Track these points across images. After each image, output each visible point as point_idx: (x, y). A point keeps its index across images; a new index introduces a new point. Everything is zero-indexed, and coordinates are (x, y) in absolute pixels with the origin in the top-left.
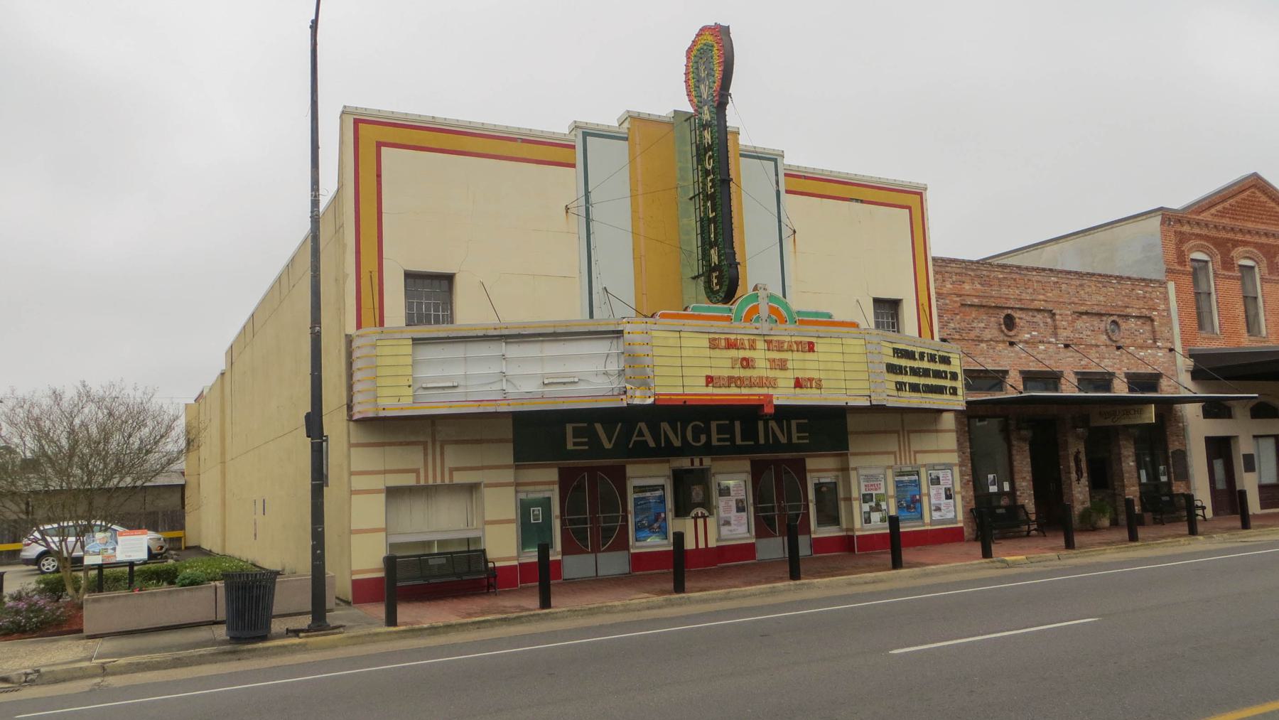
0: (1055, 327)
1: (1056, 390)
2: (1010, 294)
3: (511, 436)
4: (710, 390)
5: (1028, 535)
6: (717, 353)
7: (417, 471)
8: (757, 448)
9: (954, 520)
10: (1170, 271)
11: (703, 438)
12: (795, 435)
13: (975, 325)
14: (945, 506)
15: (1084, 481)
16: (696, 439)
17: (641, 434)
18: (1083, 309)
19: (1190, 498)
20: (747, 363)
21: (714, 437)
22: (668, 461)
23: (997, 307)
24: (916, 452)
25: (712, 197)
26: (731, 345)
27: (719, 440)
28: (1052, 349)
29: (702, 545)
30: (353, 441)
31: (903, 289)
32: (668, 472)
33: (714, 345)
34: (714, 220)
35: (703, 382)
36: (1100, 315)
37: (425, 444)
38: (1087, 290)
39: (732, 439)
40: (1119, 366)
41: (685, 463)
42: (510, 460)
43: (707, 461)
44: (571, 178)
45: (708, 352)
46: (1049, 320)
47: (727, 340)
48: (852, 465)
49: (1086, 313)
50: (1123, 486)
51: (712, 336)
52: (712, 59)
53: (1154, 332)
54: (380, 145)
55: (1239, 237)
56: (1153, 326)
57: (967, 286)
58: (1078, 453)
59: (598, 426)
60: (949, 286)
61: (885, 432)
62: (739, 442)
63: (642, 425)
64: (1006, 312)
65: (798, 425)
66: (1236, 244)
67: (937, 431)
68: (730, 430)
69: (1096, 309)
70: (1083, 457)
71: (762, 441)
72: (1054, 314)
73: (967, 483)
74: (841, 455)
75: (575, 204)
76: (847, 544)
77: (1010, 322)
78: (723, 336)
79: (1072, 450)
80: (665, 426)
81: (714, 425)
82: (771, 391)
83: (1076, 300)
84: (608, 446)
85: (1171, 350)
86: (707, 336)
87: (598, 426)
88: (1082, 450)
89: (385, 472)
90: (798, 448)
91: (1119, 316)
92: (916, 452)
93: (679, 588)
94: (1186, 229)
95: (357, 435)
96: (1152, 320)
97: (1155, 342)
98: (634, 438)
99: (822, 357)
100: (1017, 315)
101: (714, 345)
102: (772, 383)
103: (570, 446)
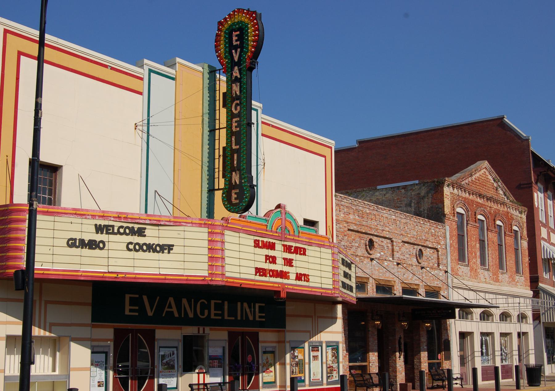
0: (393, 251)
3: (90, 301)
4: (258, 278)
6: (258, 250)
8: (235, 323)
11: (206, 312)
12: (258, 315)
13: (353, 244)
15: (402, 357)
16: (202, 313)
17: (170, 306)
18: (406, 239)
19: (450, 371)
21: (213, 312)
22: (181, 329)
25: (237, 135)
27: (131, 311)
28: (391, 264)
31: (318, 215)
32: (180, 337)
33: (257, 244)
34: (238, 151)
35: (253, 271)
38: (409, 226)
39: (222, 315)
41: (191, 330)
42: (89, 320)
43: (207, 329)
44: (138, 101)
47: (263, 241)
48: (288, 339)
49: (408, 243)
50: (420, 362)
54: (20, 54)
56: (438, 254)
57: (351, 217)
58: (400, 338)
59: (145, 298)
60: (342, 215)
61: (306, 316)
62: (226, 317)
63: (171, 300)
64: (371, 237)
65: (260, 306)
68: (219, 307)
69: (412, 241)
71: (239, 318)
73: (345, 357)
74: (278, 331)
75: (141, 123)
77: (371, 243)
79: (397, 337)
80: (184, 301)
81: (213, 302)
83: (403, 233)
84: (150, 314)
85: (446, 272)
87: (145, 298)
88: (402, 336)
90: (254, 323)
91: (423, 246)
96: (438, 251)
97: (438, 266)
99: (311, 260)
100: (375, 239)
101: (257, 244)
103: (127, 312)
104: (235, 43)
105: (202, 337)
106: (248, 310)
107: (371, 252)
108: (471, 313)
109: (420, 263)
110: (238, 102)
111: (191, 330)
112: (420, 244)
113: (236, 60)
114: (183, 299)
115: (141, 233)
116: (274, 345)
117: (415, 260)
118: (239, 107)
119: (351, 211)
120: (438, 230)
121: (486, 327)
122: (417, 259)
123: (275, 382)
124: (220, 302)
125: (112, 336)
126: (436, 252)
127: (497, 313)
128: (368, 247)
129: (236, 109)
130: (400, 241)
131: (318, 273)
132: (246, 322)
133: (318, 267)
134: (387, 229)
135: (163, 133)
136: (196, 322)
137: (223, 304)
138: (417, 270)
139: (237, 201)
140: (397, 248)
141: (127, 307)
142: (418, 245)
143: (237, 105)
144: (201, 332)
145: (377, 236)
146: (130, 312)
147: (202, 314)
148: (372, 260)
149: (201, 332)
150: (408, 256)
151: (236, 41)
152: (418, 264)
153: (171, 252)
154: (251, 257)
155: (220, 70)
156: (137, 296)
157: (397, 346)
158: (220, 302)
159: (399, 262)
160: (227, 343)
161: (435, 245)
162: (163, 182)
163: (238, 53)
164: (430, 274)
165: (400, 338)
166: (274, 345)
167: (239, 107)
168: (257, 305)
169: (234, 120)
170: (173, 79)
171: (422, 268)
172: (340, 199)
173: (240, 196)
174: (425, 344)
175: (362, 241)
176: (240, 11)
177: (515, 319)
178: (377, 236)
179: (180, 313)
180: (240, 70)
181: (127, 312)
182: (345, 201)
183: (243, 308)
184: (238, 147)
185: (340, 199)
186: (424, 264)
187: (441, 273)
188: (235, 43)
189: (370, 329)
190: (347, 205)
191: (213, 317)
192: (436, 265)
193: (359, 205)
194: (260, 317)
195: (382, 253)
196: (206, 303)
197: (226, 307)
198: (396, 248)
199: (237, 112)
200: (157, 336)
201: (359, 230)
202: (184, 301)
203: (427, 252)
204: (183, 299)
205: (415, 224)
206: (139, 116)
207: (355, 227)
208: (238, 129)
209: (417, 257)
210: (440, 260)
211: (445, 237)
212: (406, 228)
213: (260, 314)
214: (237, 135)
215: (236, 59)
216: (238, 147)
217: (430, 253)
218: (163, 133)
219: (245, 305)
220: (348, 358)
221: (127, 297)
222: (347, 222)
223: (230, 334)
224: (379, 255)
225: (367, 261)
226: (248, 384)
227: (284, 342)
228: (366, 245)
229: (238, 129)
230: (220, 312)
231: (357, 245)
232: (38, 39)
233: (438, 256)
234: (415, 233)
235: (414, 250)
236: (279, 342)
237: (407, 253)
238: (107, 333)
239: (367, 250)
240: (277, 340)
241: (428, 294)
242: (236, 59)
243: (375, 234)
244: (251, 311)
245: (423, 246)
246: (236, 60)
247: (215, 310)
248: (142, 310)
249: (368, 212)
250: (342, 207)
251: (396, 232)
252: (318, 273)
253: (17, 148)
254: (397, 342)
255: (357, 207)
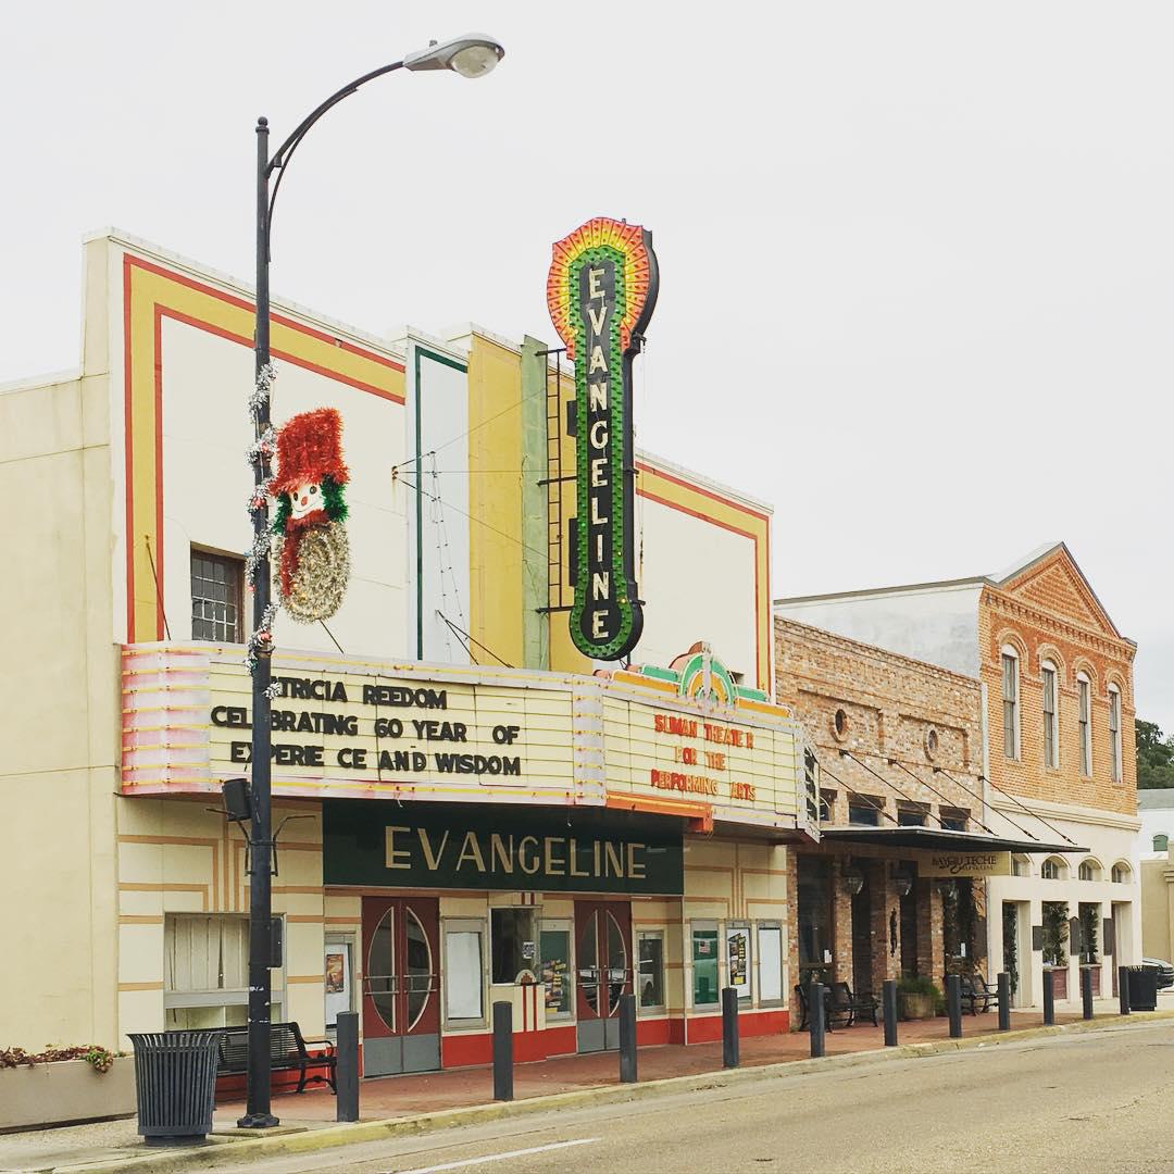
1: (876, 825)
2: (841, 680)
4: (655, 791)
5: (848, 1026)
6: (663, 737)
7: (202, 888)
8: (579, 884)
9: (780, 1003)
10: (985, 668)
11: (537, 860)
12: (631, 866)
14: (771, 976)
15: (898, 951)
17: (469, 851)
18: (906, 711)
20: (688, 756)
21: (549, 861)
22: (487, 896)
23: (831, 698)
24: (749, 901)
25: (604, 495)
26: (677, 728)
27: (397, 860)
29: (530, 1028)
30: (123, 831)
34: (606, 530)
36: (920, 721)
37: (213, 843)
39: (566, 867)
40: (931, 793)
41: (509, 900)
43: (539, 896)
45: (652, 735)
46: (875, 723)
47: (672, 719)
48: (687, 914)
50: (931, 962)
51: (659, 712)
52: (610, 287)
53: (966, 751)
54: (160, 311)
55: (1044, 629)
56: (965, 741)
57: (804, 664)
58: (894, 913)
59: (422, 832)
60: (787, 661)
62: (573, 872)
63: (471, 835)
64: (841, 706)
66: (1042, 638)
67: (769, 872)
68: (565, 854)
70: (898, 920)
71: (597, 874)
72: (881, 715)
74: (667, 900)
76: (673, 1031)
78: (669, 714)
79: (889, 912)
80: (496, 838)
81: (548, 840)
82: (710, 799)
83: (901, 697)
84: (433, 866)
86: (652, 711)
87: (422, 832)
89: (164, 887)
91: (937, 724)
92: (749, 901)
93: (504, 1093)
94: (1000, 611)
95: (130, 822)
97: (966, 765)
98: (463, 857)
100: (848, 710)
102: (702, 786)
103: (390, 864)
104: (594, 295)
105: (527, 913)
106: (501, 848)
107: (841, 738)
108: (1026, 861)
109: (932, 761)
110: (604, 424)
111: (509, 900)
112: (933, 720)
113: (598, 333)
114: (493, 835)
115: (438, 701)
116: (657, 927)
117: (923, 753)
118: (605, 436)
119: (804, 653)
120: (965, 691)
121: (1054, 890)
122: (926, 752)
123: (750, 997)
124: (562, 840)
125: (358, 913)
126: (961, 738)
127: (1074, 860)
128: (835, 726)
129: (599, 440)
130: (895, 715)
131: (769, 783)
132: (610, 882)
133: (769, 771)
134: (871, 690)
135: (452, 488)
136: (518, 882)
137: (567, 843)
138: (925, 773)
139: (606, 635)
140: (890, 729)
141: (390, 853)
142: (930, 723)
143: (601, 430)
144: (528, 902)
145: (851, 704)
146: (395, 862)
147: (530, 865)
148: (843, 753)
149: (528, 902)
150: (909, 745)
151: (597, 289)
152: (927, 763)
153: (514, 740)
154: (651, 750)
155: (558, 351)
156: (408, 830)
157: (888, 929)
158: (562, 840)
159: (894, 758)
160: (574, 924)
161: (961, 724)
162: (451, 591)
163: (602, 318)
164: (952, 783)
165: (894, 913)
166: (657, 927)
167: (605, 436)
168: (631, 846)
169: (596, 463)
170: (463, 369)
171: (936, 770)
172: (783, 628)
173: (612, 625)
174: (940, 925)
175: (825, 715)
176: (597, 224)
177: (1107, 873)
178: (851, 704)
179: (487, 863)
180: (606, 355)
181: (390, 864)
182: (793, 631)
183: (606, 854)
184: (605, 520)
185: (783, 628)
186: (940, 763)
187: (972, 781)
188: (594, 295)
189: (839, 895)
190: (797, 639)
191: (548, 871)
192: (961, 764)
193: (820, 639)
194: (636, 871)
195: (861, 740)
196: (536, 843)
197: (573, 849)
198: (888, 730)
199: (603, 445)
200: (443, 911)
201: (820, 692)
202: (496, 838)
203: (945, 738)
204: (493, 835)
205: (924, 680)
206: (404, 452)
207: (811, 686)
208: (605, 483)
209: (926, 748)
210: (970, 753)
211: (979, 707)
212: (907, 687)
213: (555, 861)
214: (604, 495)
215: (597, 328)
216: (605, 520)
217: (950, 739)
218: (452, 488)
219: (609, 846)
220: (797, 953)
221: (390, 831)
222: (796, 677)
223: (578, 905)
224: (855, 743)
225: (833, 755)
226: (612, 1008)
227: (680, 921)
228: (831, 724)
229: (605, 483)
230: (562, 862)
231: (814, 722)
232: (254, 303)
233: (966, 746)
234: (924, 699)
235: (922, 735)
236: (668, 922)
237: (905, 740)
238: (351, 907)
239: (833, 734)
240: (665, 918)
241: (904, 818)
242: (597, 328)
243: (849, 699)
244: (508, 855)
245: (937, 724)
246: (598, 333)
247: (552, 858)
248: (418, 858)
249: (836, 654)
250: (786, 644)
251: (889, 696)
252: (769, 783)
253: (165, 520)
254: (888, 922)
255: (816, 645)
